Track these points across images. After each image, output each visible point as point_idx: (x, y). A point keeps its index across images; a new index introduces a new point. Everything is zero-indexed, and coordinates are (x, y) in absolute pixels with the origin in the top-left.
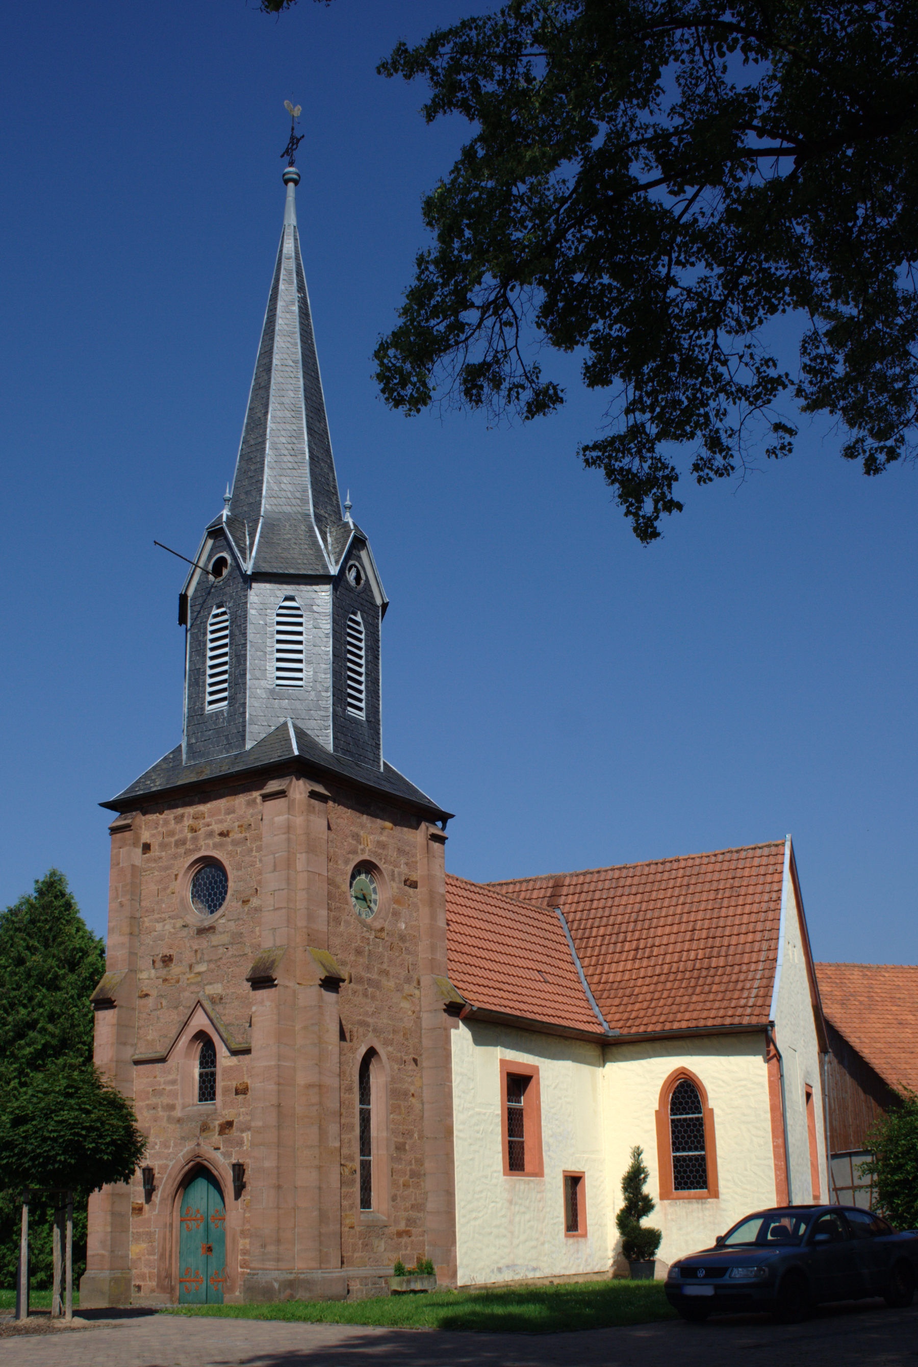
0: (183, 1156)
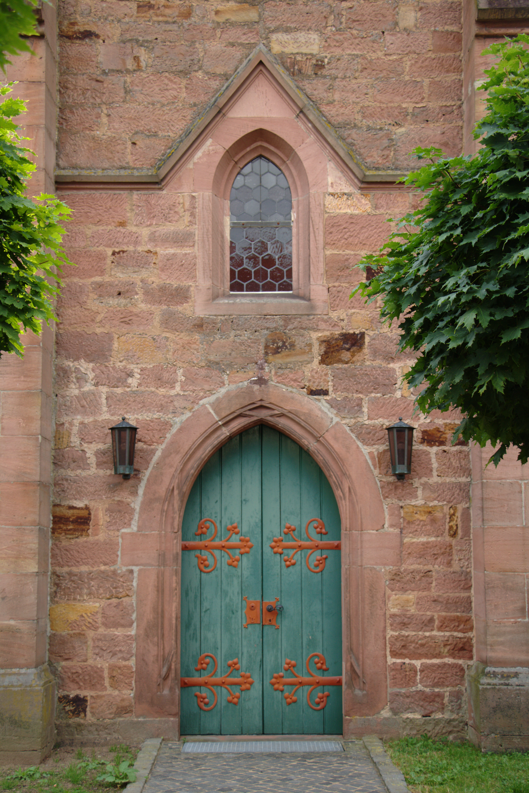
0: (216, 406)
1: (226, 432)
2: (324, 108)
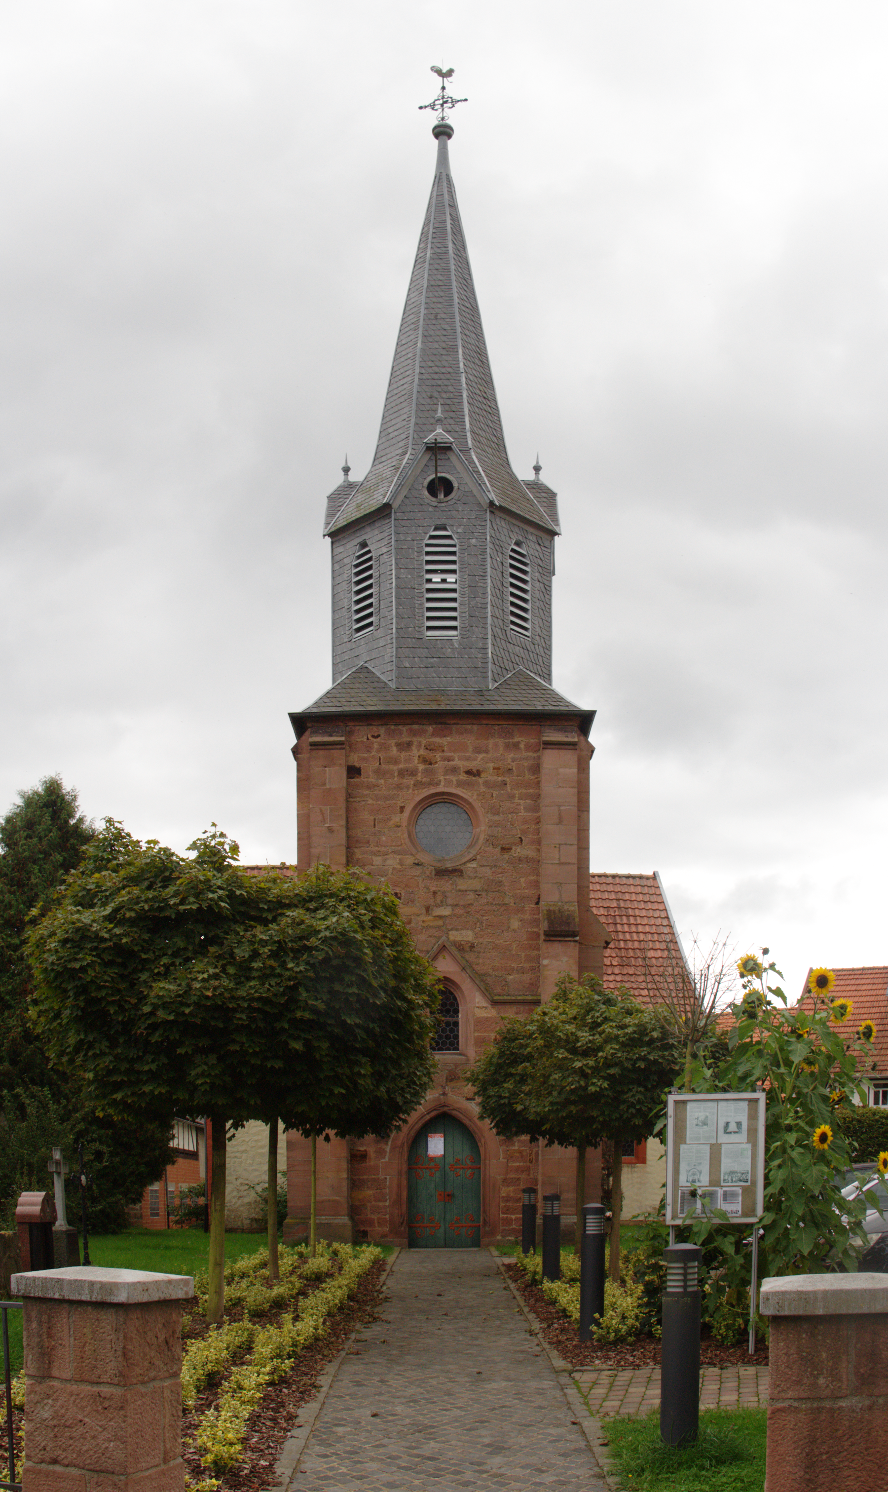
1: (428, 1117)
2: (475, 967)
